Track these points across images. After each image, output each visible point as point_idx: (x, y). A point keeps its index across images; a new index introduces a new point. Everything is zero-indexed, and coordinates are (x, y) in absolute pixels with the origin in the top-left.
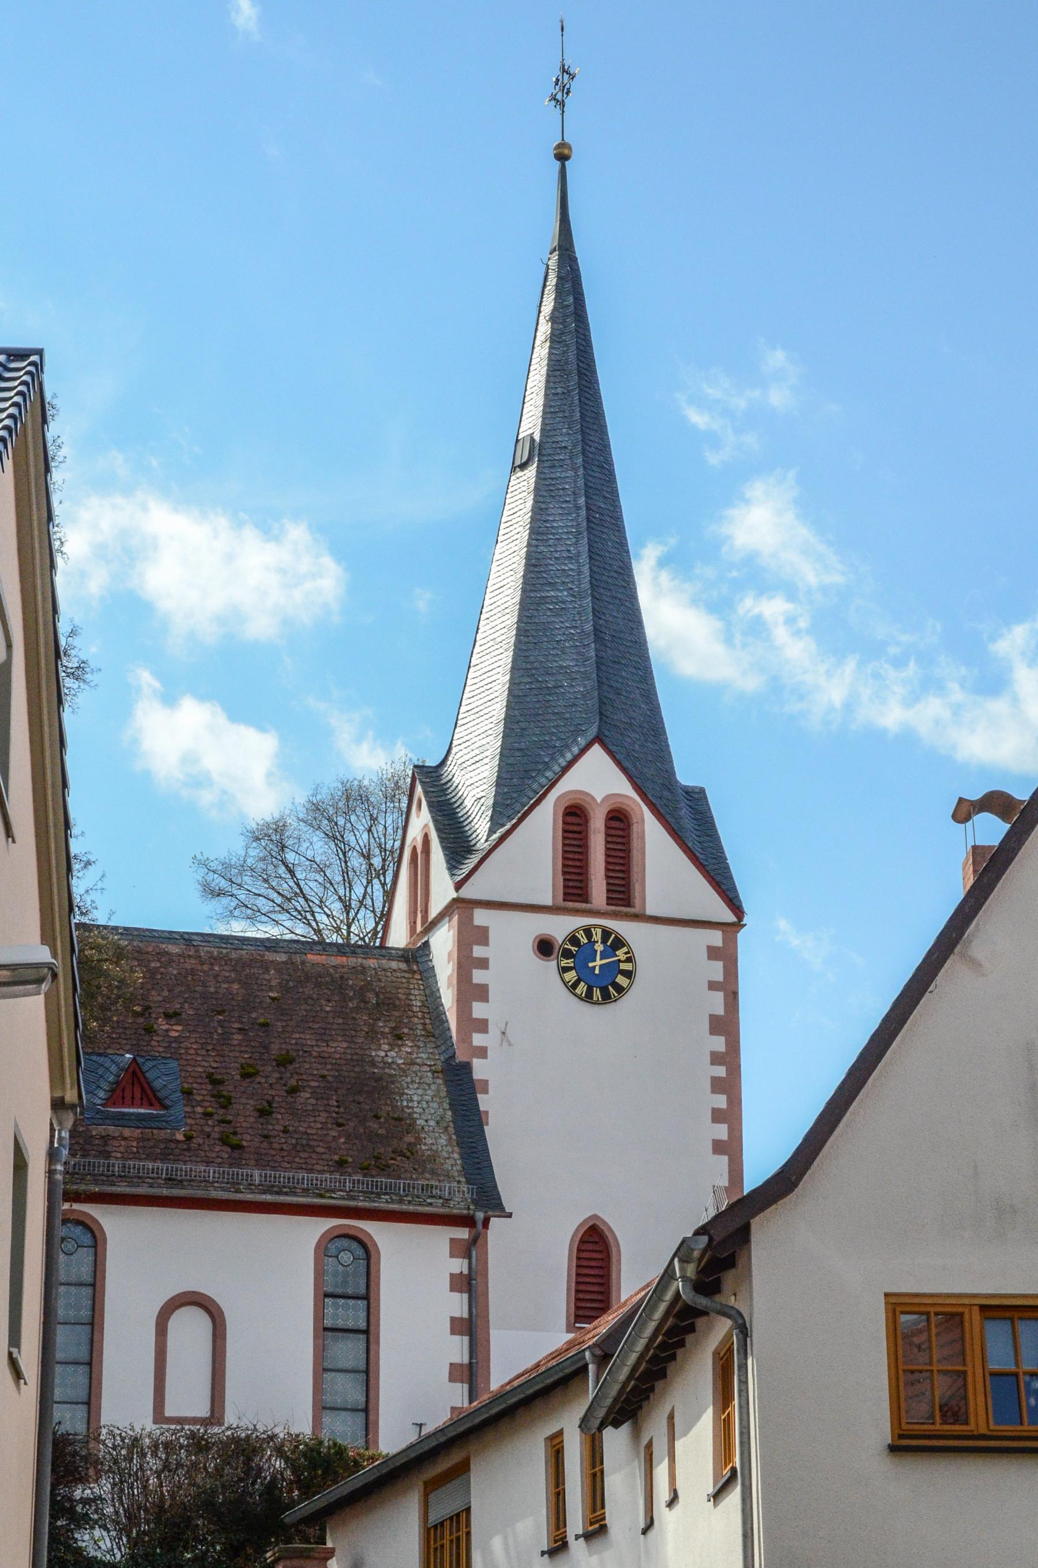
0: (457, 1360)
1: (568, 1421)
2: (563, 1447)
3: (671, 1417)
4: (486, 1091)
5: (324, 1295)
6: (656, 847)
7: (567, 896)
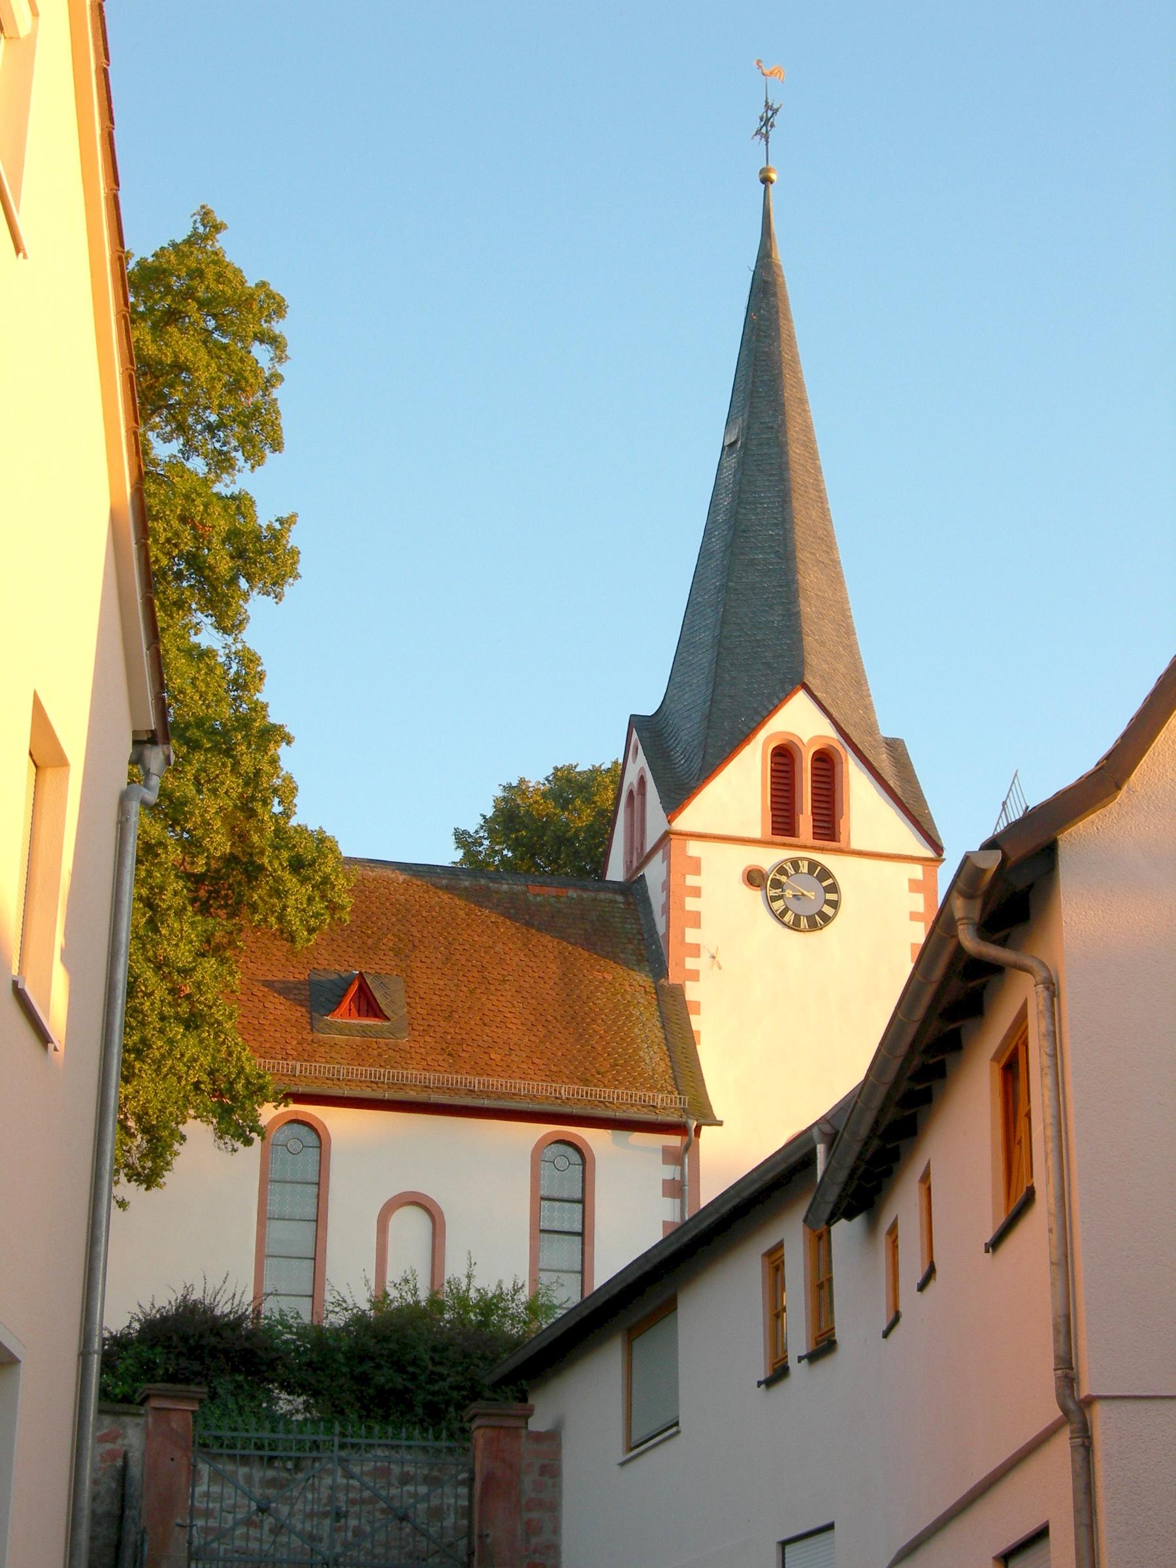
0: (669, 1219)
1: (790, 1232)
2: (783, 1262)
3: (926, 1177)
4: (698, 1012)
5: (539, 1199)
6: (861, 795)
7: (776, 830)
